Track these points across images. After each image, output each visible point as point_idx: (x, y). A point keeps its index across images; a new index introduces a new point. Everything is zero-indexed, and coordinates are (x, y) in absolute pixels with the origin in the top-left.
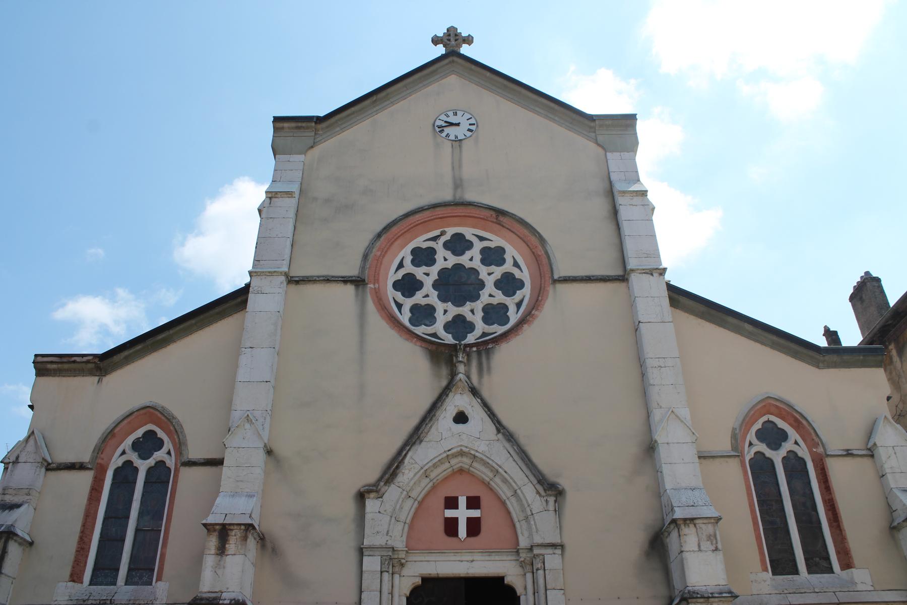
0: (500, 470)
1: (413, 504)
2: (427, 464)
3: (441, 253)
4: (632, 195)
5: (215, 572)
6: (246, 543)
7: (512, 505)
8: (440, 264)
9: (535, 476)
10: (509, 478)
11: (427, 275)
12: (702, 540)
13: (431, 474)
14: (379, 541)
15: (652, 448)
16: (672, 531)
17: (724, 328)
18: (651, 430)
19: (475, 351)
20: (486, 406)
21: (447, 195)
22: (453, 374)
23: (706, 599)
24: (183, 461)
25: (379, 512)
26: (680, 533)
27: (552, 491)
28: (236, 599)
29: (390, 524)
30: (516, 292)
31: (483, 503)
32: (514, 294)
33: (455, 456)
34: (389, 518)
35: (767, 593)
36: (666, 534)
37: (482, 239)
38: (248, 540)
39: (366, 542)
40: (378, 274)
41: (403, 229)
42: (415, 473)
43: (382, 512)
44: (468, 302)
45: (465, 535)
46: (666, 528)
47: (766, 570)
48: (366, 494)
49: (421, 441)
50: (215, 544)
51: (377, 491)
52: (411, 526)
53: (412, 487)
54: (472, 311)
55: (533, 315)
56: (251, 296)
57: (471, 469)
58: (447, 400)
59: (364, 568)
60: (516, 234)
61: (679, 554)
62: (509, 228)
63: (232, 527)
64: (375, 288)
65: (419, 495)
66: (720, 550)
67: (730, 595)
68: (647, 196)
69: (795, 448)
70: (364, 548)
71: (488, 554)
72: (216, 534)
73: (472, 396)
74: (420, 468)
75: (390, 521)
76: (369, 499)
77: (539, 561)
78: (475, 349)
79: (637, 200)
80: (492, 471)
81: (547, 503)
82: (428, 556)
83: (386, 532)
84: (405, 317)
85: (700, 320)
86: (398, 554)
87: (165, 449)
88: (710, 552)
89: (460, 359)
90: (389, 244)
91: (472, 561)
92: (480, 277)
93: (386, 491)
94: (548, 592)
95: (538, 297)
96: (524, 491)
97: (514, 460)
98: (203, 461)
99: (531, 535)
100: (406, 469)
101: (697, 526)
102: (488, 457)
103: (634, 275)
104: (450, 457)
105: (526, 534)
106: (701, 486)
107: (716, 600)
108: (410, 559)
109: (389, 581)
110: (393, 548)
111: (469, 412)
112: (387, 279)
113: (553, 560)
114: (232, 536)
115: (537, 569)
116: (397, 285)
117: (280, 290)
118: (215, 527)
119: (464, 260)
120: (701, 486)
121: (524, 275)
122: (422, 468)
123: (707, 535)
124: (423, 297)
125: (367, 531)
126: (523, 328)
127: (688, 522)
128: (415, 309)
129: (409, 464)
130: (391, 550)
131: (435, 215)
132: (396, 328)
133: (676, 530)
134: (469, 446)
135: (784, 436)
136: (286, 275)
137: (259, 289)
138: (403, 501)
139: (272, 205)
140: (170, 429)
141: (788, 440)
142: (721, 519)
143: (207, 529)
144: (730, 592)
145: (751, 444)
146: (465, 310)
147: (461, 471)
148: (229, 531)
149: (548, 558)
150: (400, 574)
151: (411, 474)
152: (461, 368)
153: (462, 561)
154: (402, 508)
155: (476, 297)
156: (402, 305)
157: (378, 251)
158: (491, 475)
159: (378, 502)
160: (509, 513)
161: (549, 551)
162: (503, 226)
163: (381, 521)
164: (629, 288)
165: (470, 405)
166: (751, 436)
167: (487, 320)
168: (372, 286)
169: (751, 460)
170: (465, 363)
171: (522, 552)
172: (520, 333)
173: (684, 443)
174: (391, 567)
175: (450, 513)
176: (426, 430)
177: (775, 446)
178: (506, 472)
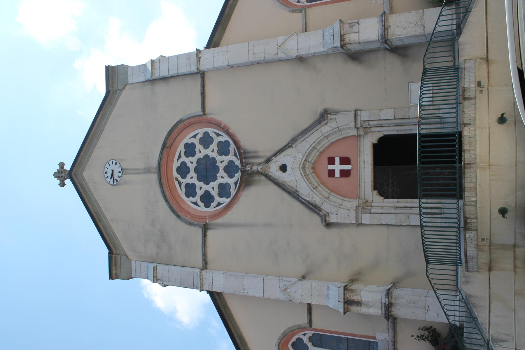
0: (313, 146)
3: (188, 180)
4: (154, 69)
5: (370, 307)
7: (333, 139)
8: (195, 181)
10: (318, 141)
11: (201, 188)
13: (315, 185)
14: (353, 214)
15: (300, 58)
17: (231, 15)
19: (245, 160)
20: (276, 154)
21: (154, 177)
22: (258, 173)
24: (309, 327)
25: (337, 215)
29: (344, 209)
30: (211, 136)
31: (332, 155)
32: (211, 138)
33: (305, 172)
34: (340, 209)
37: (180, 157)
38: (353, 289)
39: (354, 222)
40: (201, 216)
41: (175, 202)
42: (315, 195)
44: (217, 165)
46: (346, 51)
51: (325, 216)
52: (345, 196)
54: (222, 162)
55: (224, 126)
58: (273, 176)
59: (369, 223)
60: (177, 137)
61: (360, 44)
62: (173, 141)
63: (346, 298)
65: (327, 192)
66: (358, 21)
67: (383, 16)
68: (154, 60)
71: (360, 152)
72: (349, 307)
73: (271, 162)
75: (342, 208)
78: (244, 160)
79: (157, 65)
80: (313, 150)
81: (331, 119)
83: (348, 211)
84: (226, 201)
85: (227, 30)
86: (360, 204)
89: (249, 168)
90: (184, 211)
91: (364, 162)
92: (202, 157)
93: (325, 211)
95: (213, 124)
96: (325, 132)
97: (307, 138)
99: (349, 128)
100: (313, 200)
101: (345, 33)
102: (306, 153)
104: (305, 174)
105: (349, 131)
106: (321, 31)
108: (362, 196)
110: (357, 207)
111: (280, 164)
113: (364, 116)
114: (350, 298)
115: (369, 125)
116: (207, 206)
117: (211, 273)
118: (345, 308)
119: (192, 167)
120: (321, 31)
121: (201, 132)
122: (312, 190)
123: (350, 28)
124: (214, 190)
125: (348, 221)
127: (342, 39)
128: (221, 195)
131: (166, 184)
133: (347, 45)
136: (202, 270)
137: (210, 285)
139: (161, 279)
140: (291, 334)
142: (341, 20)
143: (347, 312)
144: (382, 16)
146: (221, 166)
147: (313, 168)
150: (372, 203)
151: (315, 196)
152: (255, 168)
153: (364, 168)
154: (335, 202)
155: (214, 159)
157: (187, 217)
158: (316, 151)
159: (331, 215)
160: (337, 141)
161: (358, 118)
162: (172, 144)
167: (227, 153)
172: (234, 134)
174: (367, 208)
175: (337, 174)
176: (290, 188)
178: (314, 143)
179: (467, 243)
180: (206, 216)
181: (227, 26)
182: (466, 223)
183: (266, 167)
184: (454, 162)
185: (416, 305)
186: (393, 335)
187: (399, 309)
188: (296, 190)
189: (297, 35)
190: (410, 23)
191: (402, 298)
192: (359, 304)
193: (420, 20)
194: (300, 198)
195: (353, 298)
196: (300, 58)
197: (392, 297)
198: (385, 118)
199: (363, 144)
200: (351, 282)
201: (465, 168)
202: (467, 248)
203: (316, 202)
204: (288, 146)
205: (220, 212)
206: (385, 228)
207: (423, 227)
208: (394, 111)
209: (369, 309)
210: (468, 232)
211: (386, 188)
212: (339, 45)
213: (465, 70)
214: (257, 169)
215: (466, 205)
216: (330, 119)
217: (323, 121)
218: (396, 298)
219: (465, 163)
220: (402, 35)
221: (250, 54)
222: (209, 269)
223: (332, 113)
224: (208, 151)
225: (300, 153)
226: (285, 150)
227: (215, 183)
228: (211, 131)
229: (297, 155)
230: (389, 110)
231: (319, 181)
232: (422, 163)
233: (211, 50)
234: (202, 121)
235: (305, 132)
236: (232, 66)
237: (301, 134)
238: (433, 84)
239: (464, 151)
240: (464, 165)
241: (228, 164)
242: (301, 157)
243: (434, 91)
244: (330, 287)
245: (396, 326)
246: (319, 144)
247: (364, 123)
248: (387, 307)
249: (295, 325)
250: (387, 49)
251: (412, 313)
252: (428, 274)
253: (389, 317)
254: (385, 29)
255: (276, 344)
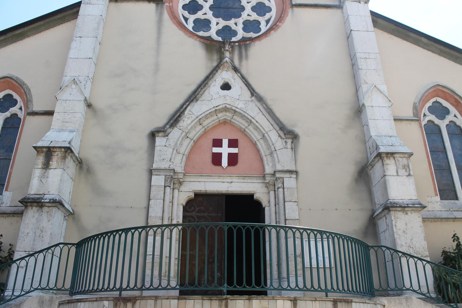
0: (253, 120)
1: (190, 142)
2: (201, 115)
5: (41, 180)
6: (65, 162)
7: (261, 145)
9: (278, 125)
10: (259, 126)
12: (400, 168)
13: (204, 123)
15: (360, 111)
16: (376, 164)
17: (407, 41)
18: (359, 100)
19: (237, 45)
20: (243, 78)
22: (221, 59)
23: (403, 208)
24: (28, 112)
25: (165, 146)
26: (384, 163)
27: (290, 135)
28: (55, 199)
29: (172, 155)
31: (240, 143)
32: (265, 15)
33: (221, 111)
34: (172, 150)
35: (439, 210)
36: (370, 167)
38: (67, 159)
39: (155, 166)
43: (167, 146)
44: (233, 18)
45: (226, 165)
46: (371, 162)
47: (437, 195)
48: (155, 133)
49: (197, 100)
50: (42, 161)
51: (164, 132)
52: (188, 158)
53: (189, 130)
54: (236, 24)
55: (278, 25)
56: (82, 5)
57: (232, 120)
58: (217, 74)
59: (152, 184)
61: (382, 178)
63: (55, 150)
64: (170, 6)
66: (412, 176)
67: (420, 206)
69: (454, 119)
70: (153, 169)
71: (243, 178)
72: (44, 154)
74: (196, 117)
75: (173, 152)
76: (158, 137)
77: (280, 182)
78: (237, 44)
80: (247, 122)
81: (286, 143)
82: (199, 178)
83: (169, 159)
84: (190, 26)
85: (391, 36)
86: (178, 175)
87: (18, 106)
88: (405, 177)
89: (227, 49)
91: (231, 182)
94: (286, 203)
96: (270, 135)
97: (263, 114)
98: (42, 112)
99: (274, 165)
100: (185, 118)
101: (396, 158)
102: (244, 112)
103: (348, 2)
104: (218, 112)
105: (271, 164)
106: (395, 134)
107: (410, 209)
108: (187, 179)
109: (170, 193)
110: (174, 170)
111: (231, 83)
112: (179, 2)
113: (289, 182)
114: (55, 156)
115: (278, 188)
118: (43, 149)
120: (395, 134)
122: (197, 117)
123: (402, 165)
124: (203, 15)
125: (156, 158)
126: (270, 33)
127: (389, 155)
128: (196, 21)
129: (188, 114)
130: (173, 171)
132: (183, 30)
133: (380, 161)
134: (231, 104)
135: (447, 112)
138: (182, 139)
140: (22, 92)
141: (450, 114)
142: (412, 154)
143: (37, 151)
144: (420, 204)
145: (425, 115)
146: (231, 23)
147: (225, 122)
148: (53, 153)
149: (286, 180)
150: (179, 190)
151: (189, 121)
152: (227, 54)
153: (224, 182)
154: (182, 145)
155: (240, 16)
156: (188, 19)
158: (246, 125)
159: (164, 139)
160: (258, 151)
161: (287, 175)
163: (166, 152)
164: (343, 12)
165: (232, 78)
166: (425, 110)
167: (245, 29)
168: (168, 4)
169: (425, 125)
170: (230, 52)
171: (268, 177)
172: (269, 36)
173: (383, 107)
174: (172, 184)
175: (216, 150)
176: (201, 93)
177: (442, 117)
178: (257, 122)
179: (95, 303)
180: (172, 3)
181: (395, 36)
182: (127, 300)
183: (229, 67)
184: (230, 283)
185: (38, 238)
186: (7, 212)
187: (34, 217)
188: (198, 100)
189: (389, 107)
190: (412, 240)
191: (49, 221)
192: (45, 166)
193: (416, 252)
194: (188, 103)
195: (54, 159)
196: (360, 111)
197: (51, 208)
198: (286, 207)
199: (253, 182)
200: (78, 160)
201: (219, 300)
202: (88, 302)
203: (183, 122)
204: (253, 92)
205: (176, 17)
206: (145, 204)
207: (125, 232)
208: (295, 220)
209: (37, 178)
210: (112, 303)
211: (197, 209)
212: (381, 150)
213: (374, 305)
214: (227, 57)
215: (156, 300)
216: (286, 141)
217: (284, 132)
218: (49, 213)
219: (229, 301)
220: (396, 228)
221: (365, 55)
222: (109, 4)
223: (293, 145)
224: (249, 10)
225: (244, 106)
226: (248, 88)
227: (212, 16)
228: (273, 14)
229: (241, 101)
230: (297, 213)
231: (208, 127)
232: (230, 230)
233: (370, 12)
234: (285, 4)
235: (270, 112)
236: (349, 37)
237: (268, 107)
238: (329, 269)
239: (249, 299)
240: (225, 299)
241: (233, 30)
242: (239, 107)
243: (321, 271)
244: (73, 133)
245: (18, 217)
246: (254, 129)
247: (280, 181)
248: (38, 201)
249: (32, 96)
250: (374, 213)
251: (28, 234)
252: (61, 246)
253: (24, 203)
254: (403, 208)
255: (11, 74)
